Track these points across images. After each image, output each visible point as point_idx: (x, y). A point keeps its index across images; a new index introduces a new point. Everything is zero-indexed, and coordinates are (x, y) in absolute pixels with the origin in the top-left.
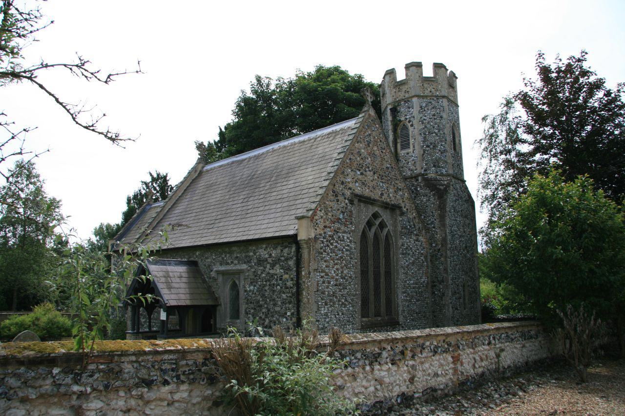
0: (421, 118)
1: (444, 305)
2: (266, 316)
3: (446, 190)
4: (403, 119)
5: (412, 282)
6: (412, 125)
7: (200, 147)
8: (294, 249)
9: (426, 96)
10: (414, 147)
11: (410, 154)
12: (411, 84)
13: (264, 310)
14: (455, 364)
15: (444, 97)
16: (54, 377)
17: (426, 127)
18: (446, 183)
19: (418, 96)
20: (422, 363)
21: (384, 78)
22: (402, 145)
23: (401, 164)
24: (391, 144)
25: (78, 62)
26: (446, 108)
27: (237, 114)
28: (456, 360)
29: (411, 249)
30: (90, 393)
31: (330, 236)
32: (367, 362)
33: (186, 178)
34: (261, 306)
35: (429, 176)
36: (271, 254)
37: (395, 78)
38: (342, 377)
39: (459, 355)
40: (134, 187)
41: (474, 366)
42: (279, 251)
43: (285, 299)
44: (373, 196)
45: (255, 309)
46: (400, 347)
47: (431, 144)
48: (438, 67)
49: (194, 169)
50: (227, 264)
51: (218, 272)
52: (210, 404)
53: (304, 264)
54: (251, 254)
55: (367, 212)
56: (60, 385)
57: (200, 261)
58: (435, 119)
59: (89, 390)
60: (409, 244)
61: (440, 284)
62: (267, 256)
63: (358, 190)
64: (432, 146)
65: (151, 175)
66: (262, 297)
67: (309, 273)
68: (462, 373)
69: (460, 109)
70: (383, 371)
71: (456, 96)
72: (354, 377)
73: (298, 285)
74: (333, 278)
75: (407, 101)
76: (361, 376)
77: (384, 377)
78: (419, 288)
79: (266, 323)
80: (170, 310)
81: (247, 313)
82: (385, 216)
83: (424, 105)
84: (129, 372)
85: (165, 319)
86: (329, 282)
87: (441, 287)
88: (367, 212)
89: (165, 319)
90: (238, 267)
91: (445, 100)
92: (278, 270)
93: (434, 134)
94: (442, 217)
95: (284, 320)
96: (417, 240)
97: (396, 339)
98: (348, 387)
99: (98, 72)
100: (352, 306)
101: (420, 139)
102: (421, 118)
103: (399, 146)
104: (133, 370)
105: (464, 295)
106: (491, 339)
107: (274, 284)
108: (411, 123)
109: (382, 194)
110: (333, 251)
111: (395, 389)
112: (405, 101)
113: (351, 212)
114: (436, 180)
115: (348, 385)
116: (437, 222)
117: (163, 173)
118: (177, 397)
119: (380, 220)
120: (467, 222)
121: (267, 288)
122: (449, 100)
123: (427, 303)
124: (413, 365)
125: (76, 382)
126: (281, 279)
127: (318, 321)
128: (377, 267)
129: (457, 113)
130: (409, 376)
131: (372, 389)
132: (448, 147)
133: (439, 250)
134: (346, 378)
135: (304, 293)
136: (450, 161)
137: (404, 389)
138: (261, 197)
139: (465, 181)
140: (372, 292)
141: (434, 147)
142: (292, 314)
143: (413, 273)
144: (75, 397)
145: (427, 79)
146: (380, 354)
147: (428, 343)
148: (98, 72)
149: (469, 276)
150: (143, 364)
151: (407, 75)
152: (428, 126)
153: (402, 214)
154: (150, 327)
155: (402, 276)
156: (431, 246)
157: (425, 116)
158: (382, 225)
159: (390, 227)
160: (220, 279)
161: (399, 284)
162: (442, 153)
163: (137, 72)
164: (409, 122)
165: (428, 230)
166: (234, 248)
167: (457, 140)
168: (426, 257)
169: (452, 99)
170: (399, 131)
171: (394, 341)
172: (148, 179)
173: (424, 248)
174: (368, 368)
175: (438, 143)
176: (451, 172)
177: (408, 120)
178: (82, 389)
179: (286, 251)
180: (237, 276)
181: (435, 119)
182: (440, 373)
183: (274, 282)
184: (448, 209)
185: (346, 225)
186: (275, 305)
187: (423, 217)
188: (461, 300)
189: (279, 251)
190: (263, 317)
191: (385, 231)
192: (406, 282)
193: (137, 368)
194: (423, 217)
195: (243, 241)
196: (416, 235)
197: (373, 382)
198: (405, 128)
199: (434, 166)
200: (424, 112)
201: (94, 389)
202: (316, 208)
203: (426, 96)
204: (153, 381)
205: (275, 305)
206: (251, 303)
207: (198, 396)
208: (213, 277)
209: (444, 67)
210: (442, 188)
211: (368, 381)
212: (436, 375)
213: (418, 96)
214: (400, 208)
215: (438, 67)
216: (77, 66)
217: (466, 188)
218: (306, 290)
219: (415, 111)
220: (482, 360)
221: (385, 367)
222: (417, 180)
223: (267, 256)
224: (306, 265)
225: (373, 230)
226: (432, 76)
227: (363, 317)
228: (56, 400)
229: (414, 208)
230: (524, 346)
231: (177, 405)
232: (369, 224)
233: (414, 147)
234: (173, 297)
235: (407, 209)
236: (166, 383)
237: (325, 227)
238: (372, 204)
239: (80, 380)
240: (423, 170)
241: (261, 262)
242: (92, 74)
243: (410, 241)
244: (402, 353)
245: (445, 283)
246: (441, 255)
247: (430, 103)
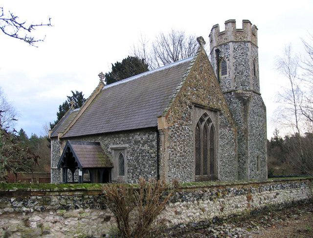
2: (140, 174)
3: (248, 100)
6: (228, 60)
7: (101, 75)
8: (156, 135)
9: (238, 42)
12: (229, 33)
13: (138, 170)
14: (248, 201)
15: (249, 42)
16: (12, 203)
17: (237, 61)
18: (248, 95)
19: (233, 42)
20: (228, 200)
21: (212, 30)
22: (222, 73)
23: (221, 84)
24: (215, 73)
25: (11, 17)
26: (250, 48)
27: (287, 137)
28: (249, 198)
30: (33, 212)
31: (177, 128)
32: (195, 199)
33: (93, 94)
34: (136, 168)
35: (238, 91)
36: (142, 138)
38: (180, 207)
39: (251, 196)
40: (63, 99)
41: (260, 203)
42: (147, 136)
44: (203, 103)
46: (215, 191)
48: (246, 22)
49: (97, 89)
50: (117, 144)
51: (112, 149)
52: (103, 220)
53: (162, 144)
54: (131, 138)
55: (200, 113)
56: (16, 207)
57: (101, 142)
59: (32, 210)
62: (140, 139)
63: (194, 99)
65: (73, 92)
67: (165, 149)
68: (253, 206)
69: (259, 50)
70: (205, 204)
71: (256, 41)
72: (188, 207)
73: (158, 156)
74: (178, 152)
75: (225, 44)
76: (192, 206)
77: (205, 207)
78: (231, 158)
80: (84, 170)
81: (128, 172)
82: (211, 115)
84: (55, 201)
85: (81, 175)
86: (176, 155)
88: (198, 114)
89: (81, 175)
90: (124, 146)
91: (249, 44)
92: (146, 147)
94: (245, 116)
98: (184, 213)
99: (24, 23)
100: (190, 168)
101: (233, 68)
103: (220, 73)
104: (57, 200)
105: (258, 163)
109: (209, 102)
110: (179, 136)
111: (212, 214)
113: (190, 113)
114: (242, 94)
115: (184, 211)
116: (242, 120)
117: (79, 91)
118: (83, 215)
119: (208, 117)
120: (261, 119)
121: (140, 158)
122: (252, 44)
123: (235, 167)
124: (223, 201)
125: (24, 205)
127: (170, 177)
129: (257, 52)
130: (220, 207)
131: (198, 214)
132: (251, 73)
134: (183, 207)
136: (252, 82)
137: (217, 214)
138: (137, 104)
139: (260, 94)
140: (202, 160)
142: (155, 172)
144: (24, 214)
145: (239, 31)
147: (232, 189)
148: (24, 23)
149: (261, 152)
150: (63, 197)
151: (226, 28)
152: (238, 60)
153: (221, 114)
154: (73, 179)
155: (220, 151)
158: (209, 121)
159: (214, 122)
160: (113, 152)
163: (48, 25)
164: (227, 58)
165: (237, 125)
166: (121, 135)
167: (256, 69)
168: (235, 140)
169: (254, 43)
170: (221, 64)
172: (71, 95)
174: (196, 202)
176: (252, 89)
178: (28, 209)
179: (151, 136)
180: (123, 151)
182: (239, 206)
183: (144, 154)
184: (249, 112)
185: (187, 121)
188: (256, 166)
189: (147, 136)
191: (211, 124)
192: (222, 154)
193: (59, 199)
195: (129, 130)
196: (229, 127)
197: (199, 210)
199: (242, 85)
201: (35, 210)
202: (169, 111)
204: (69, 206)
207: (95, 215)
208: (109, 152)
209: (250, 22)
210: (246, 98)
211: (196, 209)
212: (237, 207)
213: (233, 42)
214: (220, 111)
215: (246, 22)
216: (11, 20)
217: (261, 98)
219: (232, 49)
220: (265, 199)
221: (206, 202)
223: (140, 139)
224: (163, 144)
225: (204, 123)
227: (196, 174)
228: (14, 216)
230: (291, 192)
231: (83, 220)
232: (201, 120)
234: (86, 162)
236: (76, 207)
237: (174, 122)
238: (203, 108)
239: (27, 205)
241: (137, 142)
242: (20, 25)
243: (226, 131)
244: (217, 194)
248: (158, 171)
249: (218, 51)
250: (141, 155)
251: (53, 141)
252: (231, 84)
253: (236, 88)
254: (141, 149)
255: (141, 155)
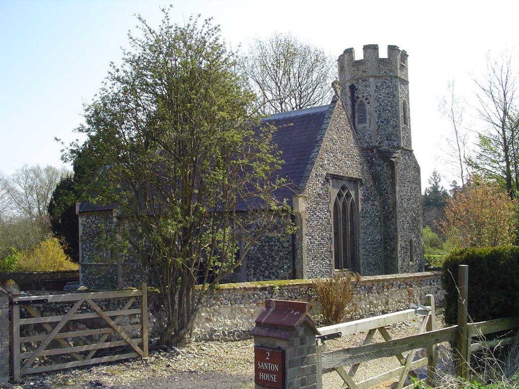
0: (377, 96)
1: (395, 258)
2: (266, 269)
4: (360, 96)
5: (369, 239)
6: (368, 103)
10: (370, 123)
11: (366, 129)
12: (369, 64)
29: (369, 212)
34: (261, 261)
37: (352, 57)
43: (283, 256)
45: (255, 264)
47: (385, 120)
48: (392, 49)
58: (388, 97)
60: (367, 208)
61: (391, 240)
63: (332, 170)
64: (385, 122)
66: (262, 255)
71: (406, 75)
78: (374, 244)
79: (266, 275)
83: (380, 84)
87: (392, 243)
93: (388, 111)
95: (282, 271)
96: (373, 205)
97: (380, 280)
101: (376, 115)
102: (377, 96)
106: (432, 281)
107: (272, 245)
108: (368, 101)
112: (363, 80)
116: (389, 189)
121: (266, 248)
126: (278, 241)
128: (345, 229)
133: (391, 212)
135: (299, 252)
141: (387, 122)
142: (289, 267)
143: (370, 233)
146: (372, 287)
147: (395, 283)
151: (364, 56)
152: (383, 104)
155: (362, 235)
156: (384, 208)
157: (380, 95)
158: (348, 195)
161: (360, 242)
162: (394, 128)
164: (366, 99)
168: (380, 219)
170: (356, 107)
171: (379, 281)
173: (378, 211)
175: (391, 119)
177: (365, 97)
181: (388, 97)
183: (272, 243)
186: (274, 260)
187: (377, 184)
190: (263, 270)
194: (377, 184)
198: (362, 104)
199: (387, 140)
200: (380, 91)
203: (381, 77)
205: (274, 260)
206: (252, 259)
213: (375, 77)
215: (392, 49)
218: (299, 249)
221: (374, 295)
222: (373, 152)
226: (387, 57)
229: (371, 178)
232: (339, 195)
233: (370, 123)
235: (366, 180)
238: (341, 179)
240: (377, 143)
245: (395, 240)
246: (393, 217)
247: (385, 82)
248: (294, 265)
249: (353, 88)
250: (267, 244)
251: (84, 219)
252: (373, 138)
253: (380, 143)
254: (268, 237)
255: (267, 244)
